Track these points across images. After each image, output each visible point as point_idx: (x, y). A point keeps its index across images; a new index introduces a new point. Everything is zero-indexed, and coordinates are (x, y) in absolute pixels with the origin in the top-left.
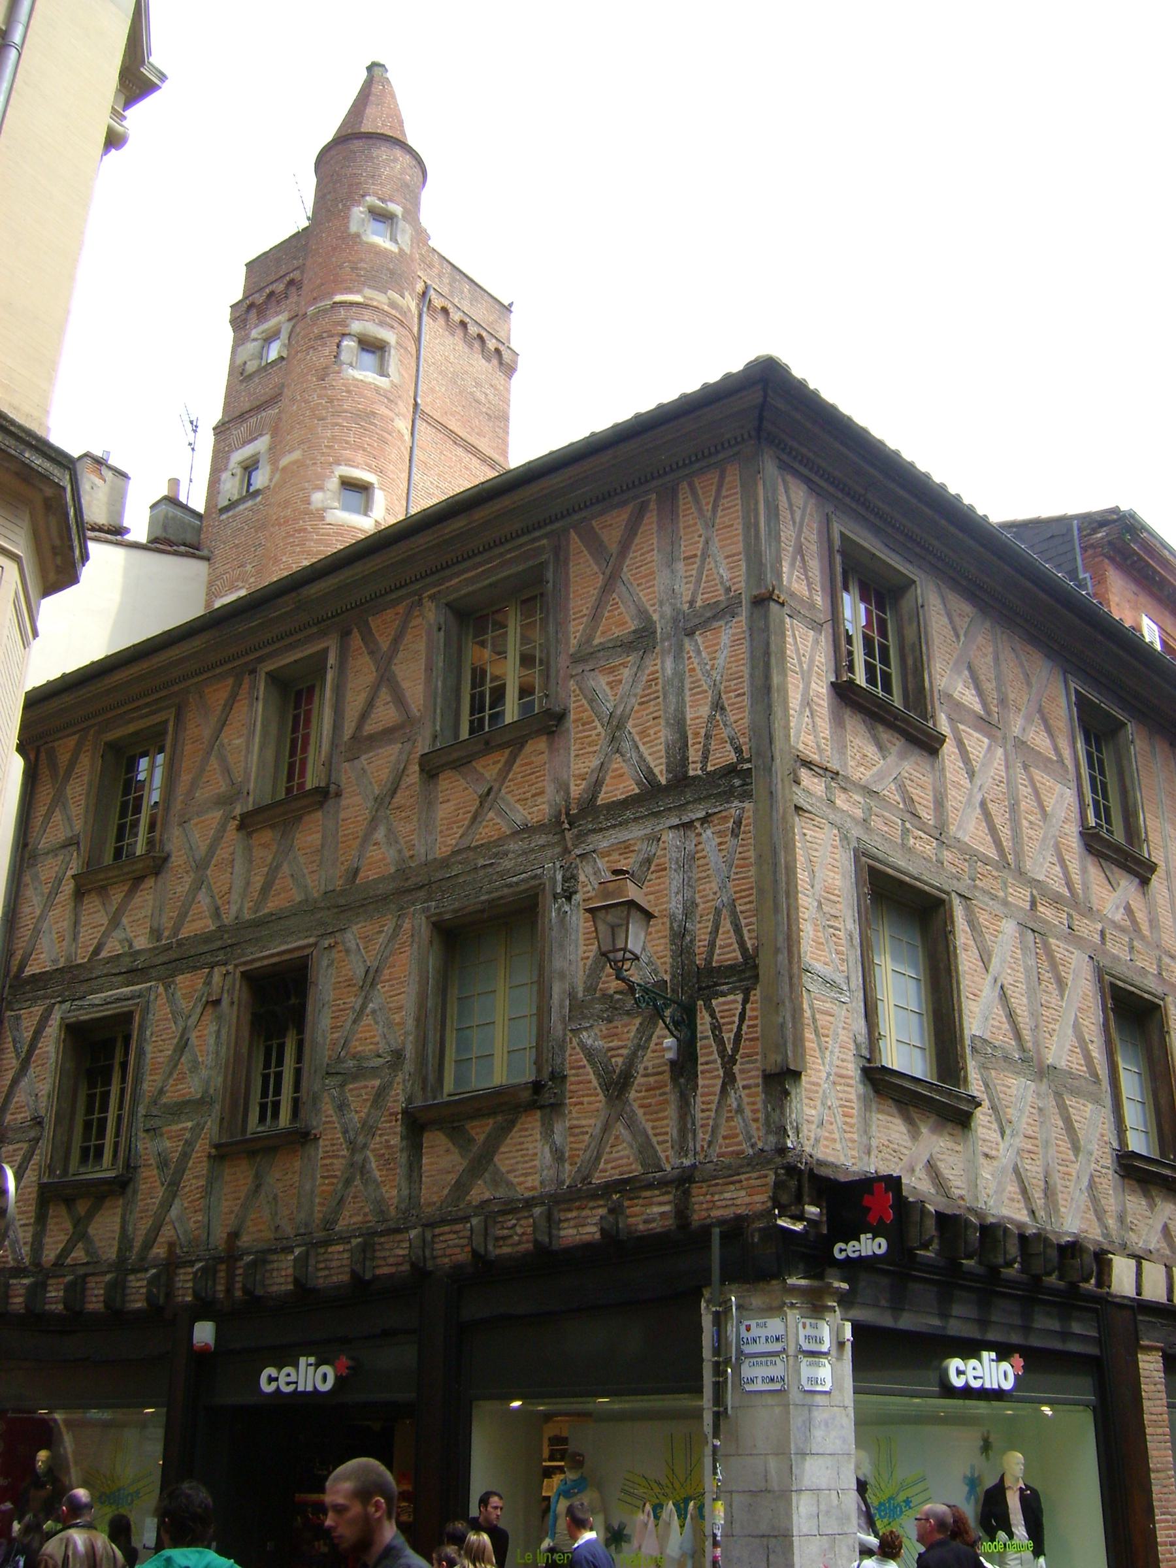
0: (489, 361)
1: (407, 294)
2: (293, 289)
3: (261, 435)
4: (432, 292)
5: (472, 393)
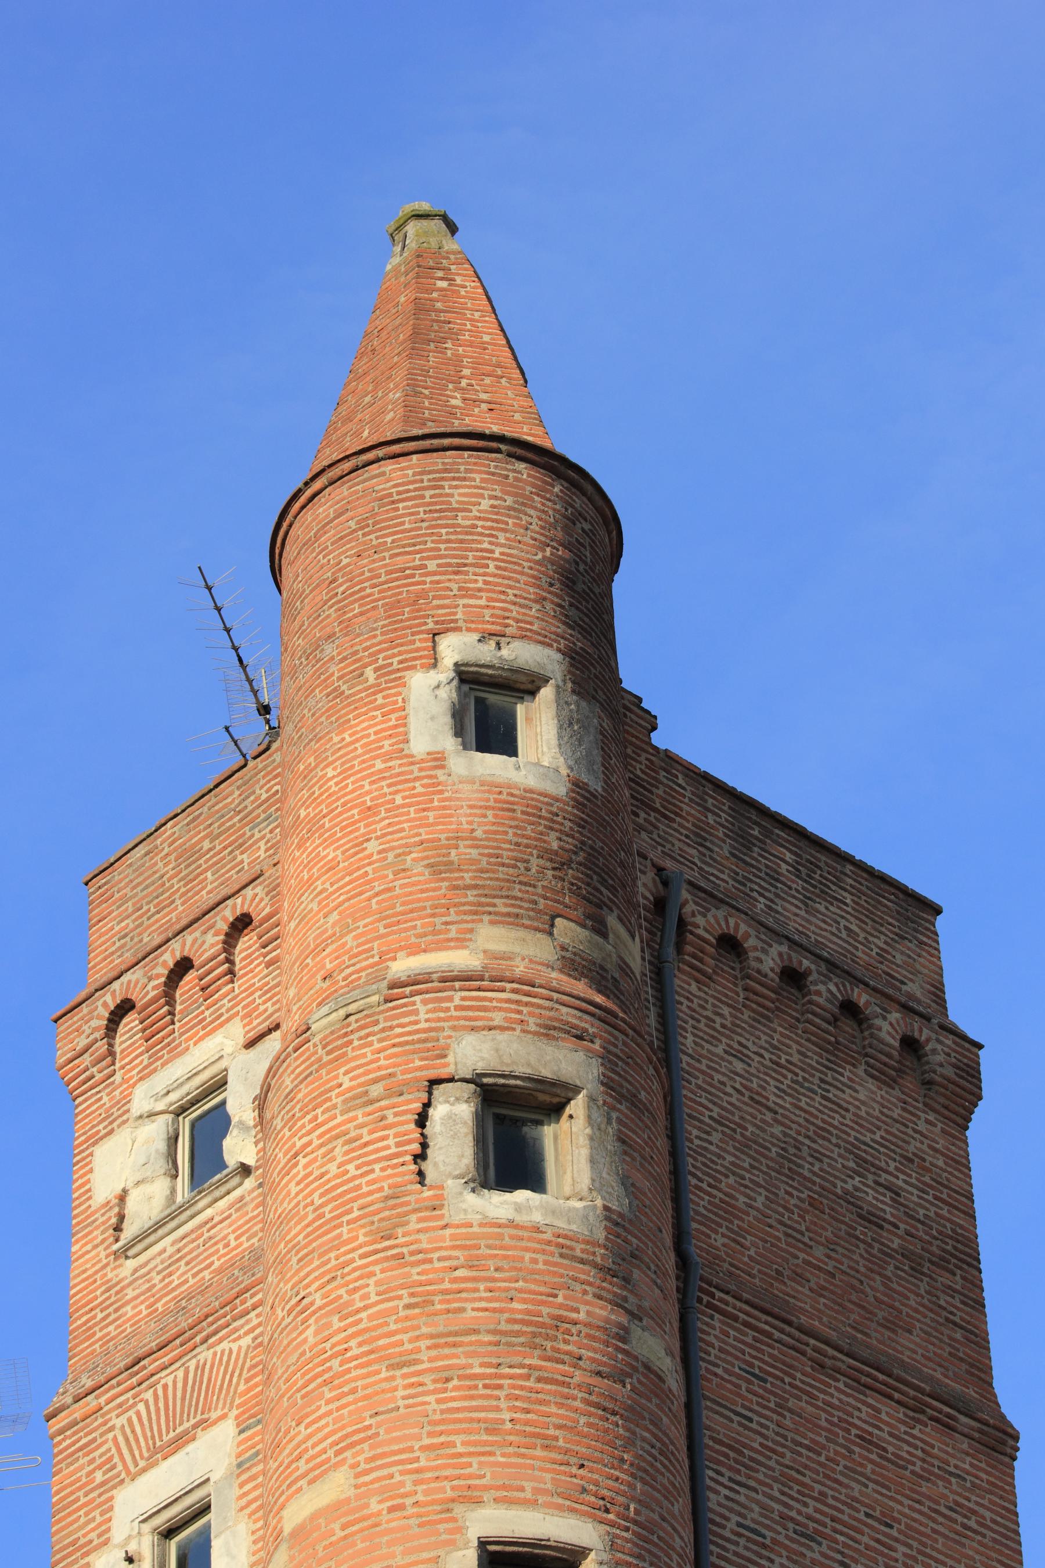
0: (890, 1082)
2: (247, 943)
3: (204, 1424)
5: (849, 1198)
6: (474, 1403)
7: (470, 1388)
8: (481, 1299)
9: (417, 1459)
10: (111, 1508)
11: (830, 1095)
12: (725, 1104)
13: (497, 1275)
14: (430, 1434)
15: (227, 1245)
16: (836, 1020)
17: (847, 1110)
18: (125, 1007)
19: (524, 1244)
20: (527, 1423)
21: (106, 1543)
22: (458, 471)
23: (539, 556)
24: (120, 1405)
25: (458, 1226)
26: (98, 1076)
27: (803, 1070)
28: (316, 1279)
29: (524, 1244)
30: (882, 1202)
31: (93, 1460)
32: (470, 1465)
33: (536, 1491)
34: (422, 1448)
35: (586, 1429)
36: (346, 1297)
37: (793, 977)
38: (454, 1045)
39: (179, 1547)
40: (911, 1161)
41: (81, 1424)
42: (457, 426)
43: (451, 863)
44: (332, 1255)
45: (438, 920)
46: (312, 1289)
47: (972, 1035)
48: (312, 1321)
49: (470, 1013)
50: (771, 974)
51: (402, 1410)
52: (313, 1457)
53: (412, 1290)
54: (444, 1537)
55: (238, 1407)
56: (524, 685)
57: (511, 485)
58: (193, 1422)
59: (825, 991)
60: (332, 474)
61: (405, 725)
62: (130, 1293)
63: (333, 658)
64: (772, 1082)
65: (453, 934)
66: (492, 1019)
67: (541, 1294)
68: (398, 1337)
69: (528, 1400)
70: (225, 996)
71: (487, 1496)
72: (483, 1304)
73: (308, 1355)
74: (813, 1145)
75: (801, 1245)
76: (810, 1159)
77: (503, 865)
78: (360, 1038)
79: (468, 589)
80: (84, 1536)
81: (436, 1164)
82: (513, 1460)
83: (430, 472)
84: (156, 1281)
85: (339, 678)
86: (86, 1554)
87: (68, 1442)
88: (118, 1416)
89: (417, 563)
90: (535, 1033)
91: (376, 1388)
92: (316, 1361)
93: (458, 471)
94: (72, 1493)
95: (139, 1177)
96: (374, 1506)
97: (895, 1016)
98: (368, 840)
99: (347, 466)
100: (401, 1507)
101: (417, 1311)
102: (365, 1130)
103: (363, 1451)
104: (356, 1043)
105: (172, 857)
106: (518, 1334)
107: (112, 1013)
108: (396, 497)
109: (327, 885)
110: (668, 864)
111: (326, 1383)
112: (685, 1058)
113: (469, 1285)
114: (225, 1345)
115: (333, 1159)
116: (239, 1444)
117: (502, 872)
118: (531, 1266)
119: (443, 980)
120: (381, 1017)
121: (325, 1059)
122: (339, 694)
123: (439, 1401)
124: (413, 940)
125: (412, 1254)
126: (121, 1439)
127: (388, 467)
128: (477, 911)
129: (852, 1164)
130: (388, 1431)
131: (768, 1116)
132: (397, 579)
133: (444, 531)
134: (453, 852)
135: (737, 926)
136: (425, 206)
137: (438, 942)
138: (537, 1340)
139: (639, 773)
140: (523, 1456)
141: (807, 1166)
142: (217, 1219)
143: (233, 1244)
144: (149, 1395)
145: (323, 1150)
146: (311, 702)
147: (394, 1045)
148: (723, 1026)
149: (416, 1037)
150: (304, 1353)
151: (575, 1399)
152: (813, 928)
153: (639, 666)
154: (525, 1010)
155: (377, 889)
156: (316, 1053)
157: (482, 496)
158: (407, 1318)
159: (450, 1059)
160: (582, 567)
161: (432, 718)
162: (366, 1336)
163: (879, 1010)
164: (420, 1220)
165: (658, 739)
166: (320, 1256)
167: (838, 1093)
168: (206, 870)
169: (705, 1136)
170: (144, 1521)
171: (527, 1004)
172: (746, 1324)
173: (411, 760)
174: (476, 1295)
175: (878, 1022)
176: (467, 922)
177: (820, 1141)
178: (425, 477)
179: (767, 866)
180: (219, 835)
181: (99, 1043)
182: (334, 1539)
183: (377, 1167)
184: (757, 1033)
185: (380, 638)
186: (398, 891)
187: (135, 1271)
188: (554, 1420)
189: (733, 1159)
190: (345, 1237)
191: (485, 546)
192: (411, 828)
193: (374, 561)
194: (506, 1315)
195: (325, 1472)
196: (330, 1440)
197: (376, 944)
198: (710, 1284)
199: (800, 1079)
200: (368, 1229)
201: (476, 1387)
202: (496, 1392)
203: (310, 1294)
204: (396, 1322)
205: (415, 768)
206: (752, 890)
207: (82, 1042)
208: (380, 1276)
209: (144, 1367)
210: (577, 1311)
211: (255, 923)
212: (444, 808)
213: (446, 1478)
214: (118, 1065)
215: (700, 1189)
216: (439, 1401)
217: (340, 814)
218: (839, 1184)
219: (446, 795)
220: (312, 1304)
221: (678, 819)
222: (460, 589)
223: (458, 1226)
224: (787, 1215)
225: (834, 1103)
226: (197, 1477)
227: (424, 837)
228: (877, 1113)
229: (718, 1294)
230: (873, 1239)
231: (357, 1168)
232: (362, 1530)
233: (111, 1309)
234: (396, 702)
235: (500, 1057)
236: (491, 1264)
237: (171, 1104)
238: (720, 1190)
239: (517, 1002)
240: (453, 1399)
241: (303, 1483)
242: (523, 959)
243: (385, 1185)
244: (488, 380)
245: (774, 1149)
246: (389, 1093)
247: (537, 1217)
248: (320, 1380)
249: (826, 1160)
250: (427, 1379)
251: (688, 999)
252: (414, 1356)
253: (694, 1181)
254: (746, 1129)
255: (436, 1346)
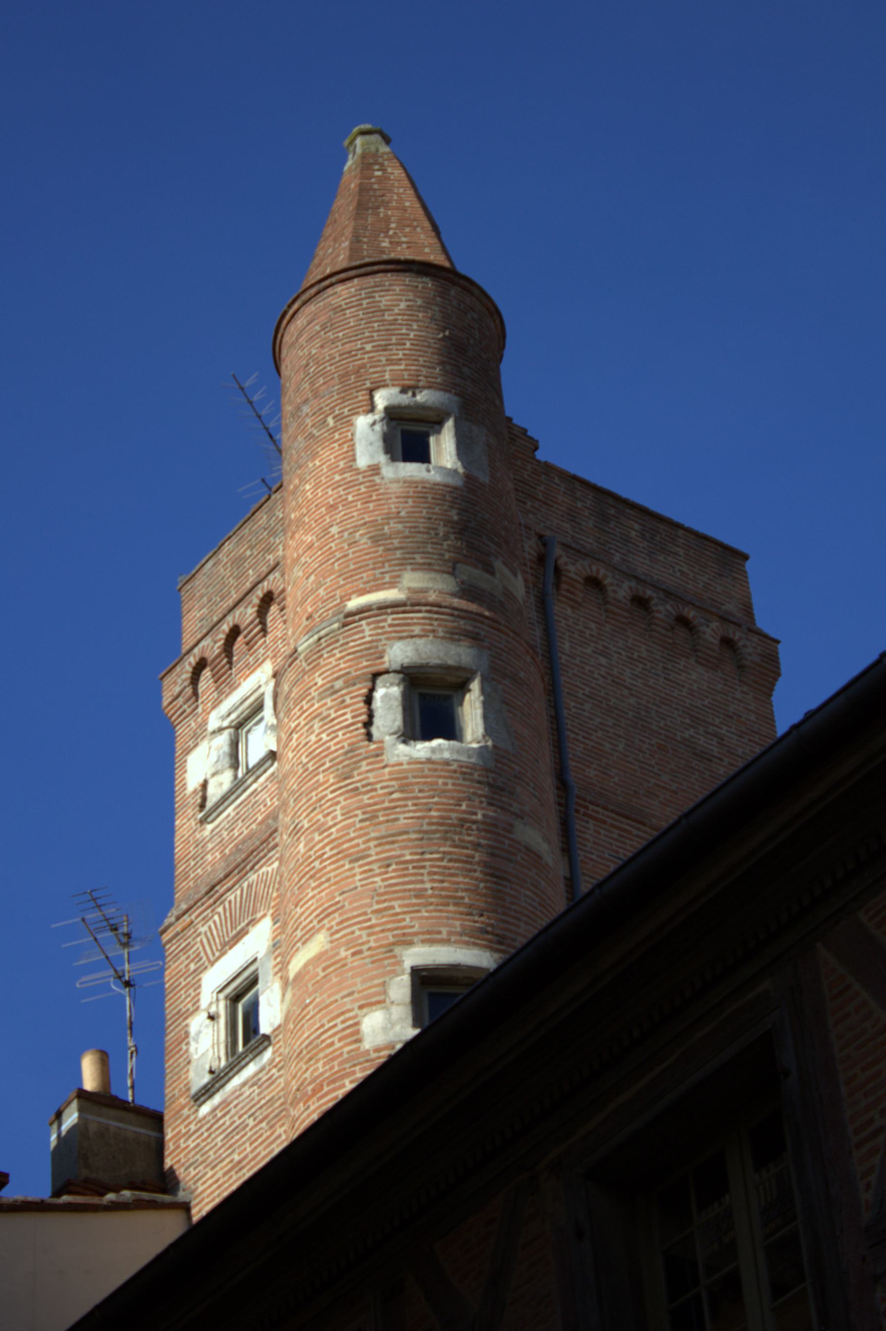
1: (498, 564)
3: (253, 922)
4: (558, 551)
6: (406, 879)
7: (403, 869)
8: (409, 811)
9: (370, 920)
10: (200, 986)
11: (671, 678)
12: (593, 685)
13: (420, 795)
14: (378, 902)
15: (265, 805)
16: (673, 628)
17: (683, 686)
18: (201, 665)
19: (438, 773)
20: (442, 889)
21: (197, 1009)
22: (384, 286)
23: (441, 336)
24: (204, 919)
25: (393, 766)
26: (189, 710)
27: (650, 662)
28: (305, 811)
29: (438, 773)
30: (711, 745)
31: (189, 957)
32: (404, 920)
33: (450, 933)
34: (374, 912)
35: (484, 891)
36: (322, 820)
37: (641, 602)
38: (388, 650)
39: (244, 1007)
40: (731, 717)
41: (182, 935)
42: (385, 257)
43: (385, 534)
44: (314, 794)
45: (377, 572)
46: (301, 818)
47: (773, 634)
48: (302, 838)
49: (398, 628)
50: (624, 600)
51: (359, 889)
52: (305, 927)
53: (364, 810)
54: (388, 968)
55: (273, 907)
56: (433, 421)
57: (421, 292)
58: (246, 921)
59: (663, 610)
60: (304, 298)
61: (353, 450)
62: (210, 846)
63: (307, 415)
64: (628, 670)
65: (387, 579)
66: (413, 631)
67: (450, 804)
68: (356, 842)
69: (443, 874)
70: (260, 646)
71: (416, 939)
72: (411, 815)
73: (301, 861)
74: (660, 710)
75: (652, 774)
76: (658, 719)
77: (420, 532)
78: (328, 652)
79: (392, 360)
80: (185, 1006)
81: (378, 727)
82: (434, 914)
83: (366, 289)
84: (224, 836)
85: (312, 426)
86: (186, 1018)
87: (174, 947)
88: (203, 925)
89: (359, 346)
90: (443, 638)
91: (343, 876)
92: (306, 864)
93: (384, 286)
94: (177, 980)
95: (213, 770)
96: (343, 953)
97: (715, 625)
98: (331, 526)
99: (313, 291)
100: (360, 952)
101: (367, 823)
102: (332, 711)
103: (334, 918)
104: (326, 656)
105: (229, 564)
106: (435, 832)
107: (194, 668)
108: (344, 307)
109: (308, 559)
110: (548, 533)
111: (311, 877)
112: (564, 657)
113: (402, 803)
114: (264, 869)
115: (313, 732)
116: (274, 931)
117: (420, 537)
118: (443, 787)
119: (380, 608)
120: (340, 637)
121: (307, 668)
122: (311, 436)
123: (383, 880)
124: (362, 586)
125: (364, 786)
126: (205, 940)
127: (339, 288)
128: (403, 564)
129: (687, 721)
130: (351, 903)
131: (626, 692)
132: (346, 358)
133: (376, 325)
134: (386, 527)
135: (598, 571)
136: (368, 126)
137: (377, 585)
138: (449, 835)
139: (526, 477)
140: (441, 911)
141: (655, 723)
142: (259, 789)
143: (269, 804)
144: (220, 909)
145: (306, 728)
146: (296, 444)
147: (349, 654)
148: (591, 635)
149: (363, 647)
150: (298, 860)
151: (475, 871)
152: (655, 571)
153: (518, 405)
154: (435, 623)
155: (338, 556)
156: (301, 666)
157: (401, 300)
158: (361, 828)
159: (386, 659)
160: (472, 341)
161: (371, 444)
162: (336, 843)
163: (703, 621)
164: (368, 764)
165: (540, 455)
166: (307, 795)
167: (677, 676)
168: (248, 569)
169: (579, 706)
170: (220, 991)
171: (437, 619)
172: (612, 825)
173: (358, 472)
174: (407, 809)
175: (703, 628)
176: (396, 571)
177: (664, 707)
178: (363, 292)
179: (620, 533)
180: (256, 545)
181: (187, 689)
182: (318, 978)
183: (340, 733)
184: (616, 639)
185: (336, 397)
186: (351, 556)
187: (213, 831)
188: (462, 886)
189: (599, 720)
190: (322, 780)
191: (404, 331)
192: (359, 515)
193: (332, 349)
194: (427, 821)
195: (312, 935)
196: (314, 914)
197: (338, 592)
198: (585, 800)
199: (648, 667)
200: (335, 774)
201: (407, 869)
202: (421, 871)
203: (300, 821)
204: (354, 831)
205: (360, 477)
206: (610, 548)
207: (177, 689)
208: (343, 803)
209: (217, 891)
210: (476, 814)
211: (275, 596)
212: (380, 500)
213: (389, 930)
214: (200, 701)
215: (577, 740)
216: (383, 880)
217: (315, 512)
218: (678, 733)
219: (381, 491)
220: (302, 827)
221: (556, 505)
222: (387, 360)
223: (393, 766)
224: (641, 755)
225: (674, 682)
226: (249, 957)
227: (367, 519)
228: (705, 688)
229: (591, 807)
230: (705, 769)
231: (328, 735)
232: (335, 970)
233: (199, 858)
234: (347, 436)
235: (419, 654)
236: (416, 788)
237: (232, 721)
238: (592, 740)
239: (430, 619)
240: (392, 878)
241: (299, 944)
242: (435, 591)
243: (345, 744)
244: (407, 230)
245: (630, 713)
246: (347, 684)
247: (447, 755)
248: (308, 876)
249: (669, 719)
250: (375, 866)
251: (565, 619)
252: (366, 853)
253: (572, 735)
254: (609, 701)
255: (380, 845)
